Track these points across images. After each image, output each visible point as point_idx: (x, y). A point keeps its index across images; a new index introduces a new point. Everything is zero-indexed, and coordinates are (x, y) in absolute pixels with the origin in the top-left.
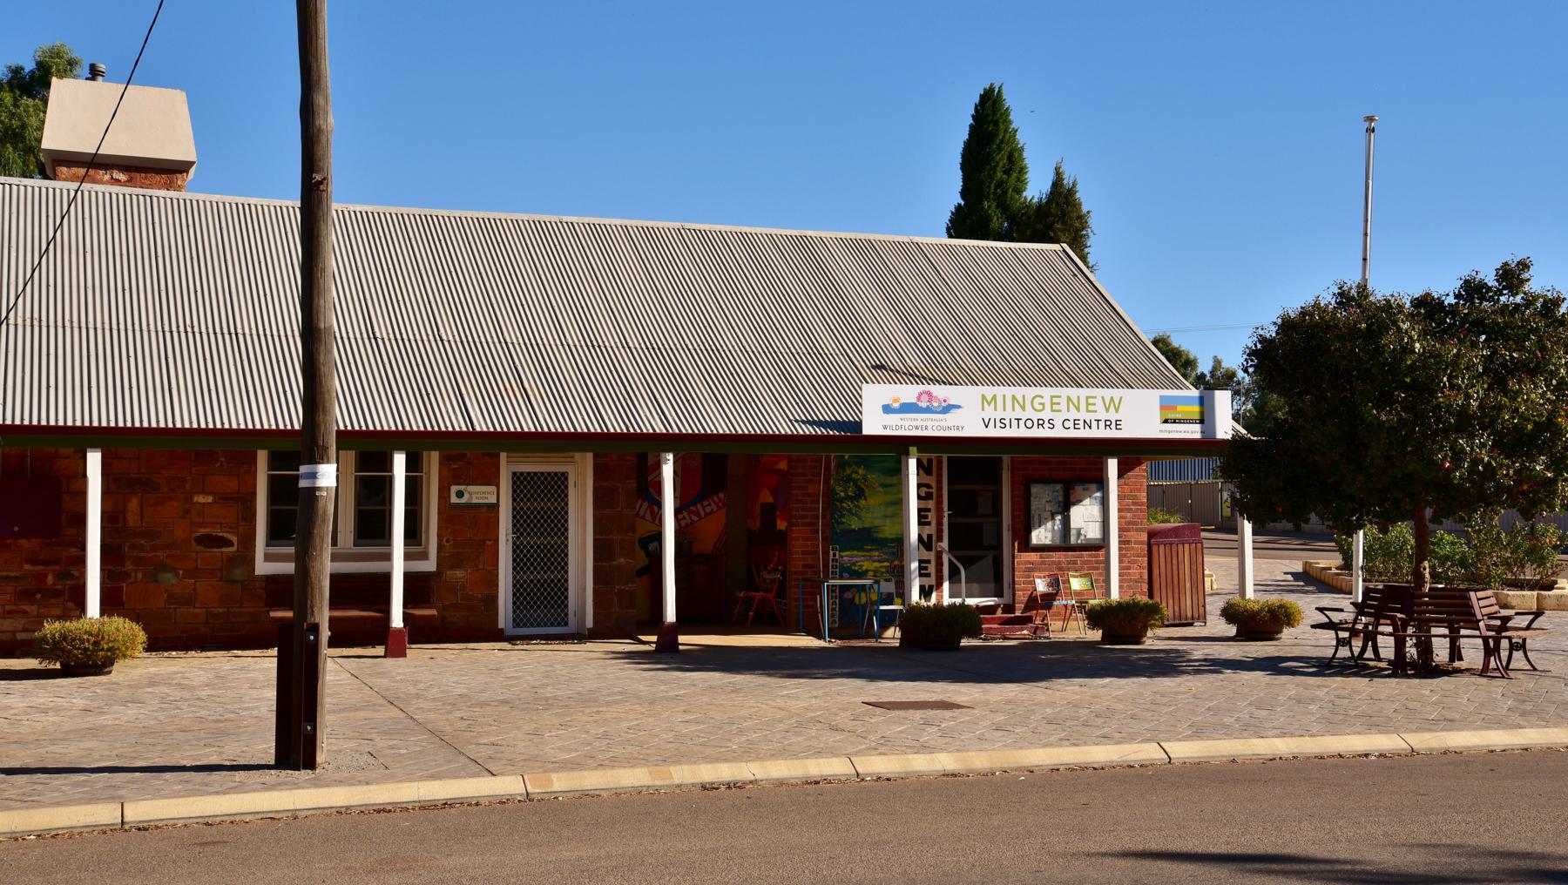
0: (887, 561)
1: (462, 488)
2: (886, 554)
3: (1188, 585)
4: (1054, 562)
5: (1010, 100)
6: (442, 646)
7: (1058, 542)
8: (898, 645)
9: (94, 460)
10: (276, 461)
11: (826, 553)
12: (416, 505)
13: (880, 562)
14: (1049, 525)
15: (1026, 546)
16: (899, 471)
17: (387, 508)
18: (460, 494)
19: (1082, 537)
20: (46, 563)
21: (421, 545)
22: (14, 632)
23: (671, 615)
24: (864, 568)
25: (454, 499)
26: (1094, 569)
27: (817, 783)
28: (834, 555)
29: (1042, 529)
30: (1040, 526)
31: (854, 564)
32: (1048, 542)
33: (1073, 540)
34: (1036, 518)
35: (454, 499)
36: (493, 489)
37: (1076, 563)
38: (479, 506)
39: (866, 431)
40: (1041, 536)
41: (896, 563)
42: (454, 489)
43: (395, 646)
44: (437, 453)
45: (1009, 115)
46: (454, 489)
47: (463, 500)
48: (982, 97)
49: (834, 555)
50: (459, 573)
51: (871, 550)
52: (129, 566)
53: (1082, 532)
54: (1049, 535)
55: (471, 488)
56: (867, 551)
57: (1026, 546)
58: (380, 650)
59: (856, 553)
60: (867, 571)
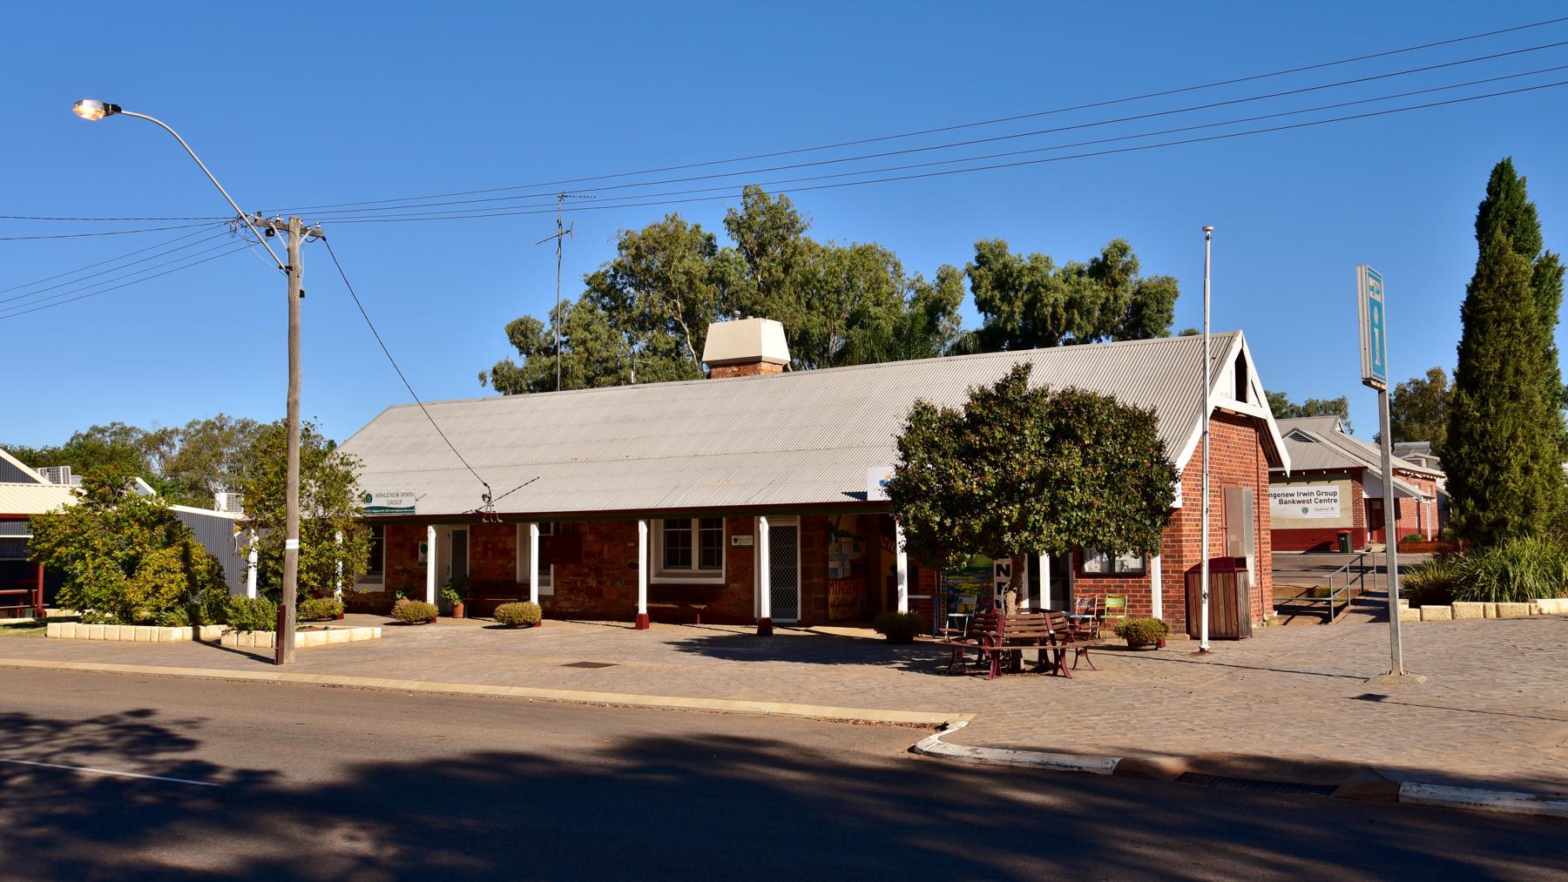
0: (978, 583)
1: (736, 536)
2: (978, 578)
3: (1222, 607)
4: (1104, 586)
5: (1519, 171)
6: (609, 623)
7: (1106, 571)
8: (756, 632)
9: (535, 532)
10: (703, 524)
11: (938, 577)
12: (704, 550)
13: (974, 583)
14: (1098, 558)
15: (1081, 574)
16: (752, 530)
17: (702, 548)
18: (736, 540)
19: (1125, 567)
20: (577, 576)
21: (664, 568)
22: (567, 608)
23: (766, 612)
24: (963, 587)
25: (733, 544)
26: (1138, 591)
27: (901, 725)
28: (944, 578)
29: (1093, 561)
30: (1091, 559)
31: (956, 585)
32: (1098, 571)
33: (1117, 569)
34: (1088, 554)
35: (733, 544)
36: (751, 537)
37: (1122, 587)
38: (744, 547)
39: (869, 499)
40: (1092, 566)
41: (985, 584)
42: (733, 537)
43: (641, 624)
44: (697, 520)
45: (1524, 186)
46: (733, 537)
47: (737, 544)
48: (1495, 172)
49: (944, 578)
50: (736, 585)
51: (968, 575)
52: (605, 578)
53: (1125, 563)
54: (1099, 566)
55: (741, 537)
56: (966, 576)
57: (1081, 574)
58: (633, 625)
59: (957, 577)
60: (965, 589)
